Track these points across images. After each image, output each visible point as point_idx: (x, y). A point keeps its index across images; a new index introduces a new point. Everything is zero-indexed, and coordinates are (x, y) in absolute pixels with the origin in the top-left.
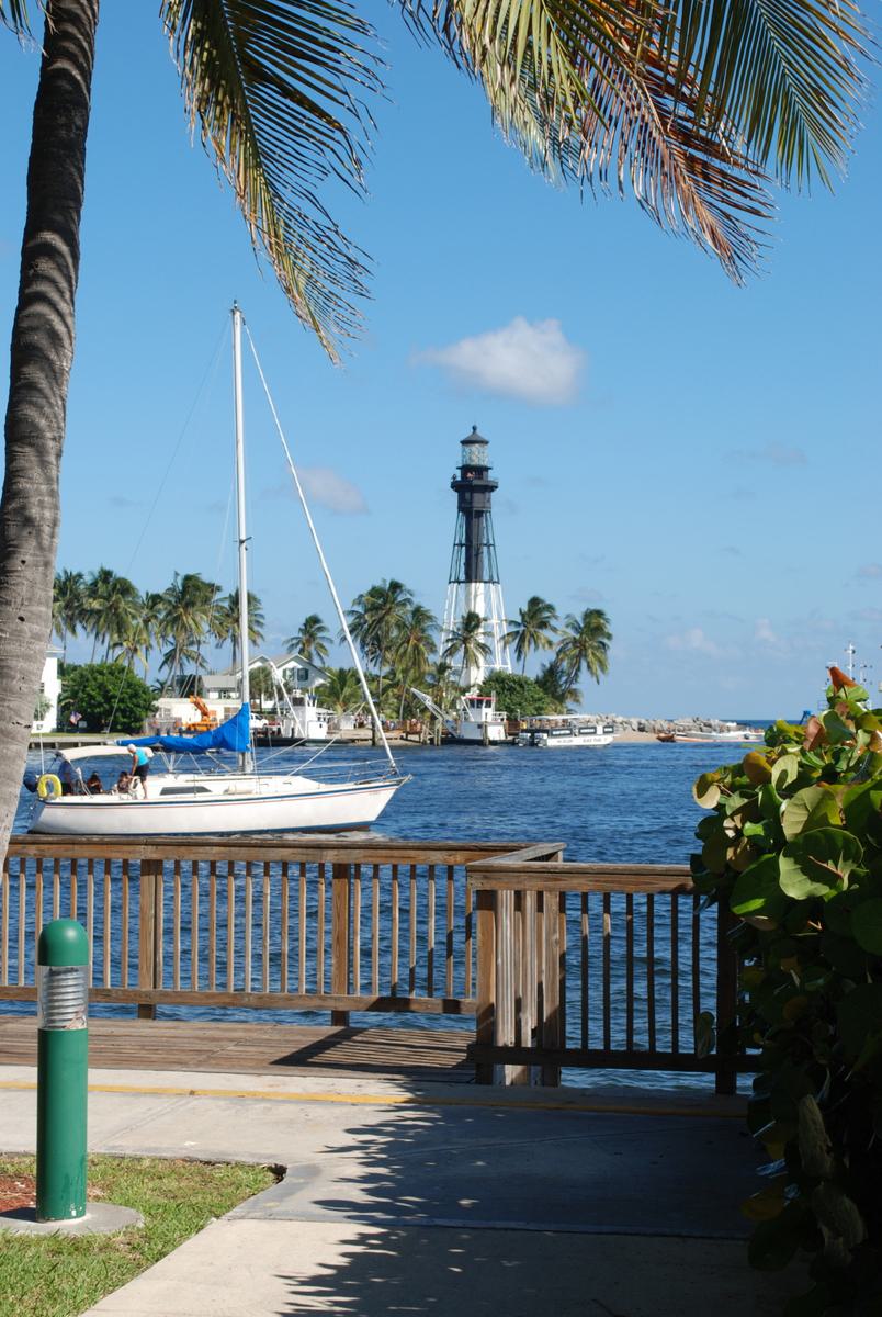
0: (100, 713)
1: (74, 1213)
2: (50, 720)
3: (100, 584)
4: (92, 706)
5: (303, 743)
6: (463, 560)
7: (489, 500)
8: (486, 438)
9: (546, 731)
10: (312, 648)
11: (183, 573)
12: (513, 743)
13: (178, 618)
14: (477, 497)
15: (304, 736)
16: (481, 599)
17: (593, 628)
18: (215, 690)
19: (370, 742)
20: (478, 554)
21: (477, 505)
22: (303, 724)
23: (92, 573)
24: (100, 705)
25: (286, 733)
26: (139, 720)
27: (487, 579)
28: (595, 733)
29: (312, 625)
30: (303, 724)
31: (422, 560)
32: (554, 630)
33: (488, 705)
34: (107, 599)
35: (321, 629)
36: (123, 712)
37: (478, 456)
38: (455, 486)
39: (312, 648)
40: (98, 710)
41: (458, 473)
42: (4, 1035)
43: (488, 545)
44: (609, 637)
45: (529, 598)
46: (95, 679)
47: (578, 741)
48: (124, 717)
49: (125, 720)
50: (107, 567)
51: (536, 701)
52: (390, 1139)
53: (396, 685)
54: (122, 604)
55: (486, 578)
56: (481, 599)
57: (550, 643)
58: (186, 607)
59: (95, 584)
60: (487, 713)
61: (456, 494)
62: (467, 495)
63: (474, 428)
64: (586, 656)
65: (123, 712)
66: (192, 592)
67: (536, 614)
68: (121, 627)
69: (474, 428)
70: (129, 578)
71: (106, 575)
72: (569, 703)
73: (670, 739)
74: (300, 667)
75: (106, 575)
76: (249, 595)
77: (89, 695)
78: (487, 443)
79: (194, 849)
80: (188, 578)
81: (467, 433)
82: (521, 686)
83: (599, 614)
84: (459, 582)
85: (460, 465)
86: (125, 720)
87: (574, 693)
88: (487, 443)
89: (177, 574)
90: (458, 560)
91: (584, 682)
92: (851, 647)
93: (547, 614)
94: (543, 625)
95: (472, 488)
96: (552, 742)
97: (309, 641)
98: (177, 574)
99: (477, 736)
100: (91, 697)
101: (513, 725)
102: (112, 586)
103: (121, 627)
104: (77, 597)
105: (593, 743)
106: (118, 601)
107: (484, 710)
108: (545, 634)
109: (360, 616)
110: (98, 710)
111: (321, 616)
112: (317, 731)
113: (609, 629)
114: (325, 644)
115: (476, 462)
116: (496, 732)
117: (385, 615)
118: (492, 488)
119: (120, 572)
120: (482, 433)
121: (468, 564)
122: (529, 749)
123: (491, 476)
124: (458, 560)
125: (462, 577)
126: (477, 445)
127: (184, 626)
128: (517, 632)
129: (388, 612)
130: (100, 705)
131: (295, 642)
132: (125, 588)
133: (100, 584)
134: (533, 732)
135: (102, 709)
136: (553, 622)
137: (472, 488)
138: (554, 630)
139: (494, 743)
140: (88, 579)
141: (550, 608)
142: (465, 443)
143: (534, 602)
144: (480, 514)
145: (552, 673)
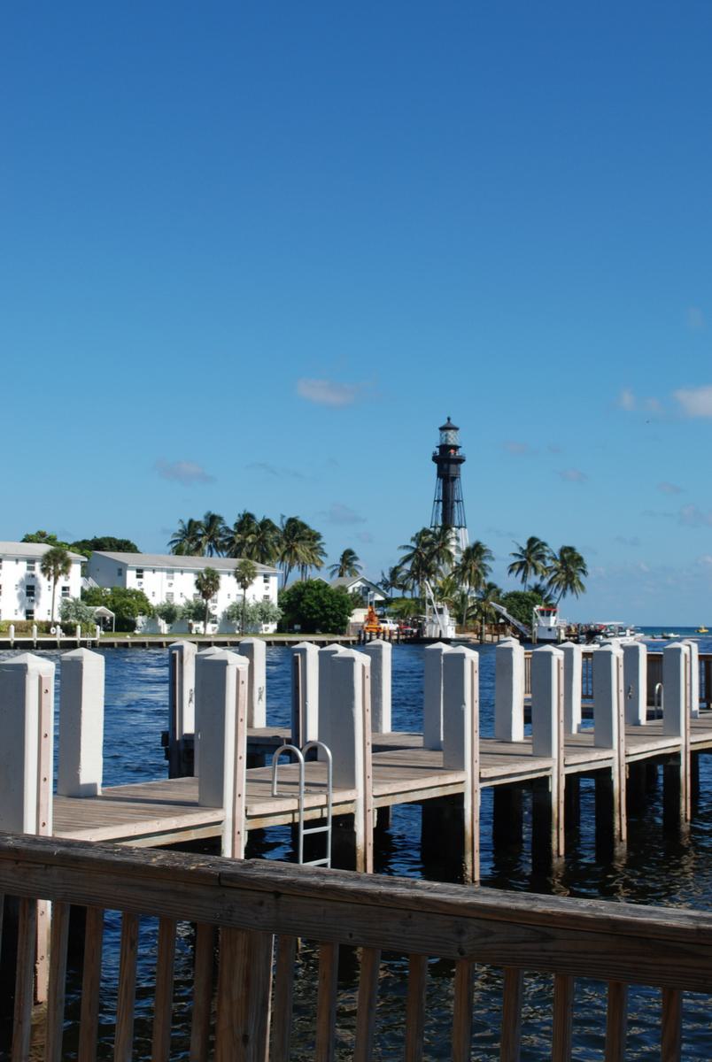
0: (316, 619)
1: (71, 971)
2: (273, 627)
6: (440, 512)
7: (459, 469)
11: (288, 517)
14: (453, 467)
24: (316, 612)
27: (457, 524)
28: (625, 635)
35: (356, 559)
37: (453, 439)
38: (435, 459)
40: (314, 616)
41: (438, 450)
43: (458, 501)
45: (528, 538)
48: (334, 622)
49: (335, 624)
50: (215, 512)
55: (457, 524)
61: (436, 465)
62: (445, 466)
63: (449, 419)
65: (334, 618)
69: (449, 419)
74: (364, 585)
79: (135, 714)
80: (291, 521)
81: (444, 423)
85: (439, 445)
86: (335, 624)
89: (283, 517)
90: (437, 511)
95: (447, 461)
100: (310, 607)
110: (314, 616)
111: (354, 550)
115: (452, 442)
118: (460, 461)
120: (454, 422)
124: (437, 511)
126: (452, 431)
127: (296, 554)
128: (521, 562)
131: (335, 568)
135: (318, 615)
137: (447, 461)
142: (443, 429)
143: (532, 541)
144: (454, 479)
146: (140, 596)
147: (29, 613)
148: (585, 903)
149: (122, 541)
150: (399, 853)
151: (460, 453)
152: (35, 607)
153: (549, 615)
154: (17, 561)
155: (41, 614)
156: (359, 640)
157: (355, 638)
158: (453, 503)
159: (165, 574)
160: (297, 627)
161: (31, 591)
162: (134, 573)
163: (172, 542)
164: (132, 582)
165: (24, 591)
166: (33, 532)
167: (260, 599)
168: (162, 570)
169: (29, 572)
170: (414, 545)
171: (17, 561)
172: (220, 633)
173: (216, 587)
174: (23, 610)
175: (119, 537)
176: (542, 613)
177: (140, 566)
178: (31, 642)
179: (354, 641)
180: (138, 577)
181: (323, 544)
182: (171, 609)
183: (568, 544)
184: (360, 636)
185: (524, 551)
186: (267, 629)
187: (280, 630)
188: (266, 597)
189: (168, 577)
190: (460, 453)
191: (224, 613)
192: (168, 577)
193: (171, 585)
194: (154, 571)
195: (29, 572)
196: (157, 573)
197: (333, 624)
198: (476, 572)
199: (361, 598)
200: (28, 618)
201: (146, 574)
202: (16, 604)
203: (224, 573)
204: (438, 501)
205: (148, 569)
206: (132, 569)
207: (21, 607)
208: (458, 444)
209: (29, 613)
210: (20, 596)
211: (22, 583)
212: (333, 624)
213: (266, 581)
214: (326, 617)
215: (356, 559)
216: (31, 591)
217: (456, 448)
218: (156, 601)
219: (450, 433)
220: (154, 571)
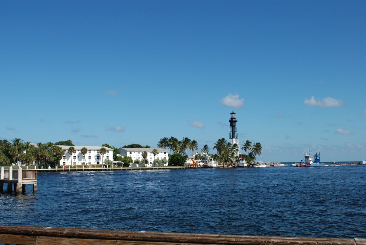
2: (167, 164)
3: (171, 140)
4: (175, 161)
5: (212, 167)
6: (231, 134)
8: (235, 113)
9: (255, 165)
10: (206, 150)
12: (249, 167)
13: (185, 145)
14: (234, 123)
15: (212, 166)
16: (235, 141)
17: (258, 147)
18: (190, 158)
19: (223, 167)
20: (234, 133)
21: (234, 125)
22: (212, 164)
23: (169, 138)
24: (177, 161)
25: (209, 165)
26: (184, 164)
27: (236, 138)
29: (206, 147)
30: (212, 164)
31: (225, 134)
32: (251, 146)
33: (244, 160)
34: (173, 142)
35: (208, 147)
36: (181, 162)
37: (234, 116)
39: (206, 150)
42: (0, 214)
43: (236, 132)
44: (261, 147)
46: (175, 156)
47: (261, 166)
51: (249, 159)
52: (51, 228)
53: (224, 157)
54: (176, 143)
55: (236, 138)
56: (235, 141)
57: (251, 149)
58: (186, 143)
59: (170, 139)
60: (244, 162)
61: (230, 123)
62: (232, 123)
63: (233, 111)
64: (257, 151)
65: (181, 162)
66: (187, 140)
67: (248, 143)
68: (176, 147)
69: (233, 111)
70: (177, 138)
71: (172, 138)
72: (254, 160)
73: (273, 166)
75: (172, 138)
76: (102, 146)
77: (175, 159)
78: (235, 114)
80: (186, 138)
82: (246, 157)
83: (259, 143)
84: (230, 138)
87: (255, 158)
88: (235, 114)
89: (184, 138)
91: (257, 156)
92: (309, 148)
93: (250, 143)
94: (249, 145)
95: (233, 122)
96: (256, 166)
97: (205, 149)
98: (184, 138)
99: (242, 166)
101: (248, 163)
102: (174, 140)
103: (176, 147)
104: (167, 142)
105: (263, 167)
106: (175, 142)
107: (243, 161)
108: (250, 147)
109: (217, 144)
111: (207, 145)
112: (214, 165)
113: (261, 146)
114: (208, 150)
115: (233, 117)
116: (246, 165)
117: (220, 144)
118: (236, 121)
119: (175, 137)
121: (232, 135)
122: (252, 168)
123: (236, 119)
125: (231, 138)
128: (244, 147)
129: (222, 144)
130: (177, 161)
132: (176, 140)
133: (171, 140)
134: (253, 165)
136: (251, 145)
137: (233, 122)
138: (251, 146)
139: (245, 167)
140: (169, 139)
141: (250, 142)
142: (231, 114)
143: (247, 141)
144: (234, 126)
145: (251, 154)
146: (130, 158)
147: (98, 163)
148: (362, 240)
149: (138, 145)
150: (33, 225)
151: (236, 119)
152: (99, 161)
153: (242, 160)
154: (95, 151)
155: (101, 163)
156: (187, 167)
157: (186, 167)
158: (234, 132)
159: (137, 153)
160: (173, 165)
161: (98, 157)
162: (129, 153)
163: (158, 144)
164: (128, 155)
165: (97, 158)
166: (124, 146)
167: (163, 158)
168: (136, 152)
169: (98, 153)
170: (217, 143)
171: (95, 151)
172: (152, 166)
173: (146, 155)
174: (96, 162)
175: (137, 144)
176: (241, 159)
177: (131, 151)
178: (101, 169)
179: (185, 168)
180: (165, 154)
181: (243, 145)
182: (137, 161)
183: (71, 140)
184: (187, 166)
185: (245, 144)
186: (165, 165)
187: (169, 165)
188: (165, 158)
189: (138, 153)
190: (236, 119)
191: (153, 162)
192: (138, 153)
193: (139, 155)
194: (134, 152)
195: (98, 153)
196: (135, 153)
197: (180, 164)
198: (229, 150)
199: (200, 157)
200: (98, 164)
201: (132, 153)
202: (95, 161)
203: (149, 152)
204: (231, 132)
205: (133, 152)
206: (128, 152)
207: (96, 161)
208: (235, 117)
209: (98, 163)
210: (95, 159)
211: (96, 156)
212: (180, 164)
213: (165, 154)
214: (179, 162)
215: (208, 147)
216: (98, 157)
217: (235, 118)
218: (134, 159)
219: (233, 115)
220: (134, 152)
